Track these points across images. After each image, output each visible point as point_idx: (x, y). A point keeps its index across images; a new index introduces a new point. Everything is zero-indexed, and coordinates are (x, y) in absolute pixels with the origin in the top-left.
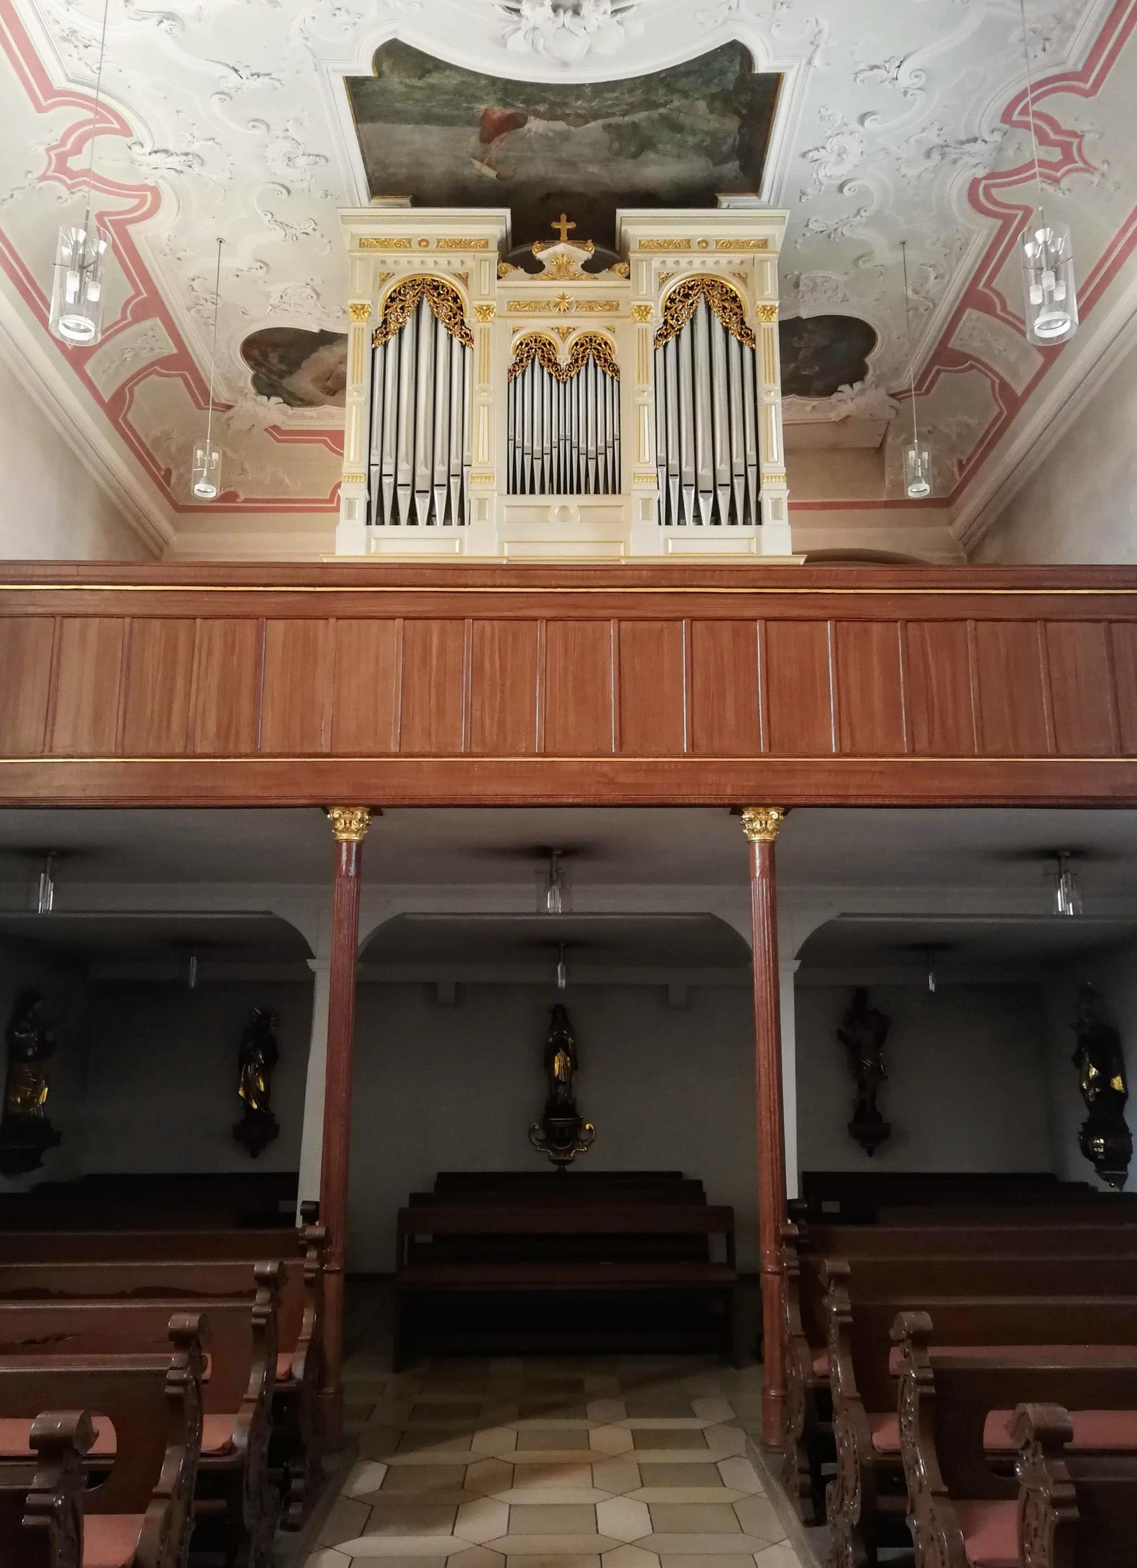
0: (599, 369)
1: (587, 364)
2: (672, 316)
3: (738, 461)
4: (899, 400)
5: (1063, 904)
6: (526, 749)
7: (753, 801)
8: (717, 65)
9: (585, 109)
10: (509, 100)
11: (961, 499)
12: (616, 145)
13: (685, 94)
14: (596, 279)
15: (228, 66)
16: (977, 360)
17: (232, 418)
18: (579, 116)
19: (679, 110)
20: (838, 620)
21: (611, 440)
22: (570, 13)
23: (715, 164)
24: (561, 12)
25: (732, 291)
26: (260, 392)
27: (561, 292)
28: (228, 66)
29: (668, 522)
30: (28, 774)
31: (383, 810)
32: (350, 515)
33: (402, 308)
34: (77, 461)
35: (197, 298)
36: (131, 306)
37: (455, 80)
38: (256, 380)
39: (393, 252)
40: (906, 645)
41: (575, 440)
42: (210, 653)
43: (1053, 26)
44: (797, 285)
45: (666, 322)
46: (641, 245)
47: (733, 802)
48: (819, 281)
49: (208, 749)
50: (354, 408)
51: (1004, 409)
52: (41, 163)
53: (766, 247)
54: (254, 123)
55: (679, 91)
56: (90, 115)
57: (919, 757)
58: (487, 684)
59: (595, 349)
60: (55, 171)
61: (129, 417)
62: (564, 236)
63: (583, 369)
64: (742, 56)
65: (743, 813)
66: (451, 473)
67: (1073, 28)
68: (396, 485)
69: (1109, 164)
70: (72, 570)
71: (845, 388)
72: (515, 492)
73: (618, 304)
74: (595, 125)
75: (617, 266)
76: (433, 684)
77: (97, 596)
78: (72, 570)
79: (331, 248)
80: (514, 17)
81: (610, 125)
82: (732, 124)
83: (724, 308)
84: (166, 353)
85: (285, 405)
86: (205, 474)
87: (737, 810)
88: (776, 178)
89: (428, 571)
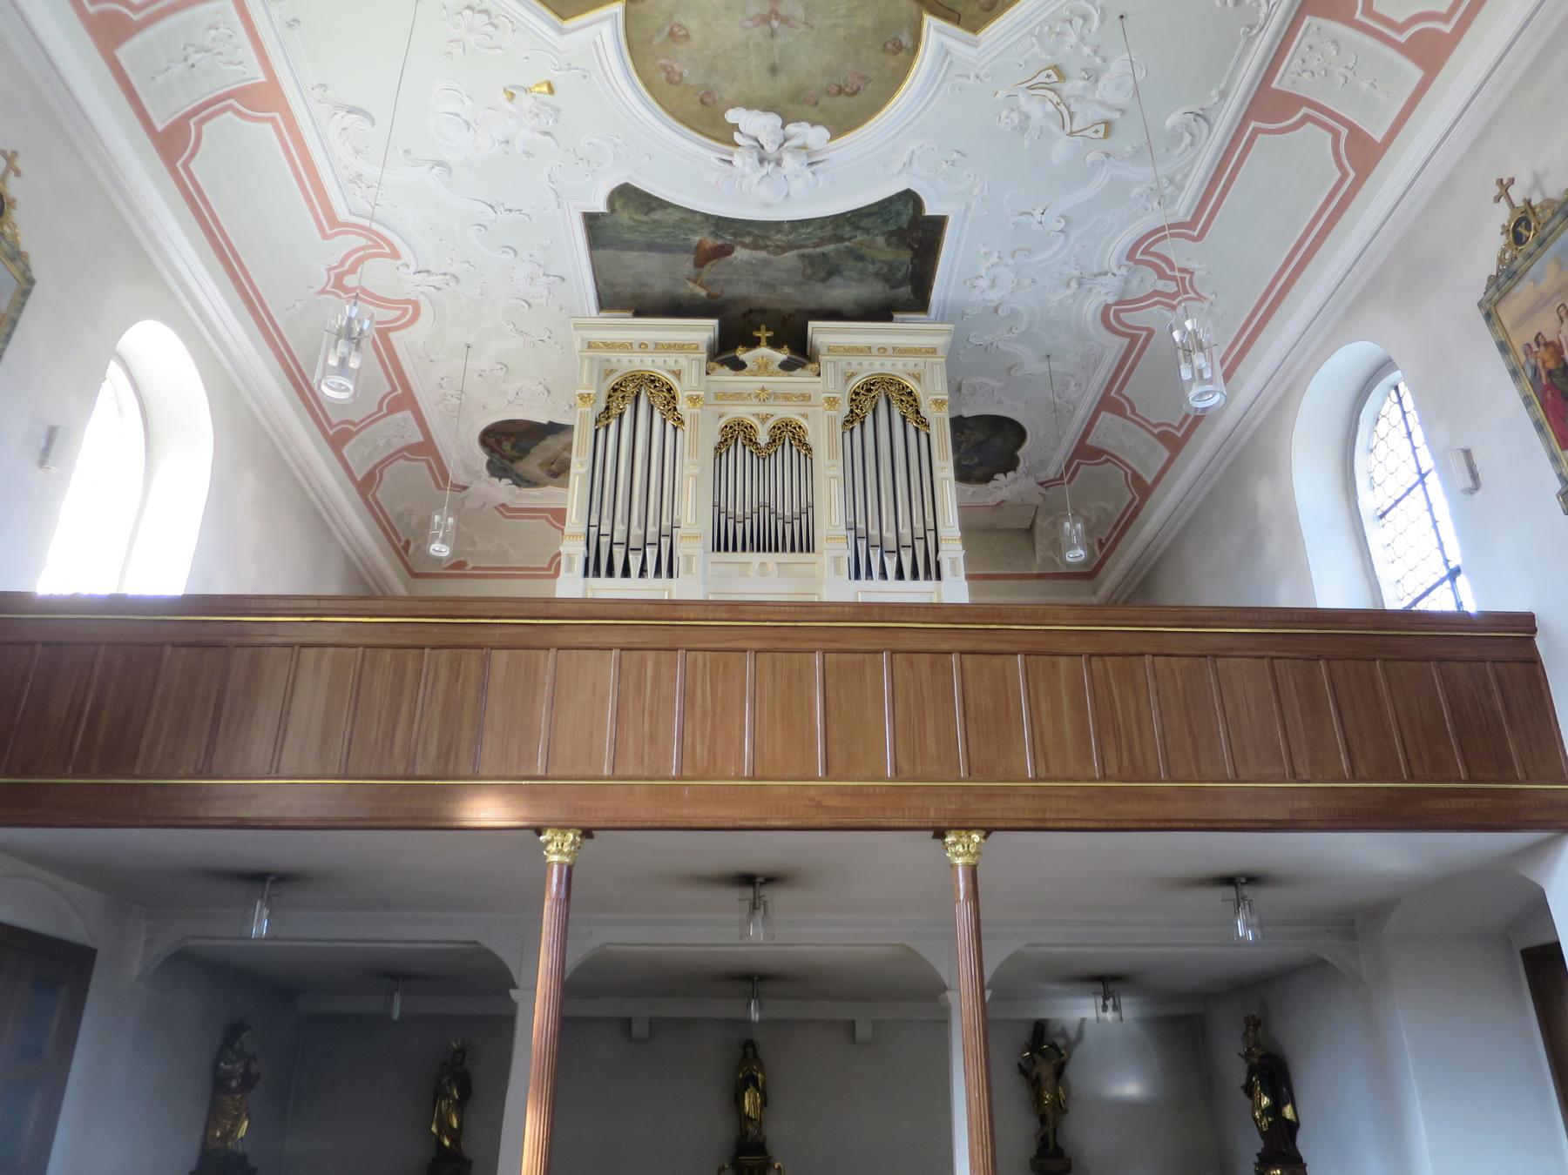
0: (794, 448)
1: (783, 444)
2: (857, 407)
3: (918, 525)
4: (1046, 488)
5: (1243, 930)
6: (735, 773)
7: (956, 825)
8: (893, 208)
9: (784, 241)
10: (720, 233)
11: (1102, 573)
12: (809, 271)
13: (867, 231)
14: (792, 376)
15: (486, 203)
16: (1112, 455)
17: (466, 497)
18: (778, 246)
19: (861, 243)
20: (1027, 654)
21: (798, 511)
22: (772, 165)
23: (892, 288)
24: (766, 163)
25: (908, 387)
26: (493, 475)
27: (760, 385)
28: (486, 203)
29: (857, 576)
30: (253, 793)
31: (594, 832)
32: (570, 569)
33: (623, 397)
34: (328, 530)
35: (445, 394)
36: (387, 400)
37: (675, 217)
38: (490, 464)
39: (617, 352)
40: (1091, 677)
41: (773, 506)
42: (436, 678)
43: (1166, 185)
44: (959, 389)
45: (852, 411)
46: (829, 350)
47: (937, 825)
48: (978, 387)
49: (428, 771)
50: (577, 477)
51: (1136, 495)
52: (322, 280)
53: (936, 353)
54: (505, 249)
55: (862, 229)
56: (362, 241)
57: (1110, 782)
58: (698, 714)
59: (791, 431)
60: (332, 287)
61: (378, 495)
62: (763, 342)
63: (780, 448)
64: (914, 200)
65: (945, 837)
66: (662, 533)
67: (1183, 188)
68: (612, 544)
69: (1216, 295)
70: (314, 604)
71: (1000, 476)
72: (719, 550)
73: (810, 396)
74: (792, 255)
75: (810, 366)
76: (646, 711)
77: (333, 627)
78: (314, 604)
79: (563, 353)
80: (727, 166)
81: (803, 255)
82: (905, 256)
83: (902, 401)
84: (414, 441)
85: (514, 486)
86: (441, 536)
87: (940, 834)
88: (941, 307)
89: (645, 606)
